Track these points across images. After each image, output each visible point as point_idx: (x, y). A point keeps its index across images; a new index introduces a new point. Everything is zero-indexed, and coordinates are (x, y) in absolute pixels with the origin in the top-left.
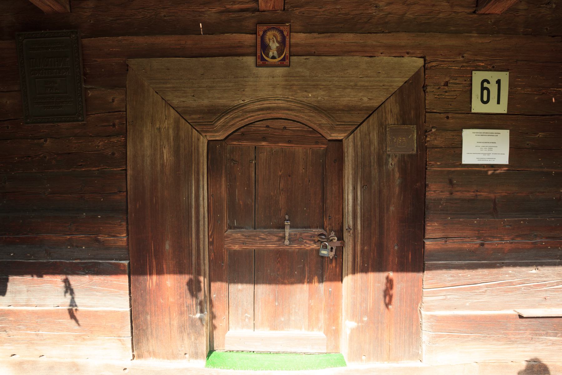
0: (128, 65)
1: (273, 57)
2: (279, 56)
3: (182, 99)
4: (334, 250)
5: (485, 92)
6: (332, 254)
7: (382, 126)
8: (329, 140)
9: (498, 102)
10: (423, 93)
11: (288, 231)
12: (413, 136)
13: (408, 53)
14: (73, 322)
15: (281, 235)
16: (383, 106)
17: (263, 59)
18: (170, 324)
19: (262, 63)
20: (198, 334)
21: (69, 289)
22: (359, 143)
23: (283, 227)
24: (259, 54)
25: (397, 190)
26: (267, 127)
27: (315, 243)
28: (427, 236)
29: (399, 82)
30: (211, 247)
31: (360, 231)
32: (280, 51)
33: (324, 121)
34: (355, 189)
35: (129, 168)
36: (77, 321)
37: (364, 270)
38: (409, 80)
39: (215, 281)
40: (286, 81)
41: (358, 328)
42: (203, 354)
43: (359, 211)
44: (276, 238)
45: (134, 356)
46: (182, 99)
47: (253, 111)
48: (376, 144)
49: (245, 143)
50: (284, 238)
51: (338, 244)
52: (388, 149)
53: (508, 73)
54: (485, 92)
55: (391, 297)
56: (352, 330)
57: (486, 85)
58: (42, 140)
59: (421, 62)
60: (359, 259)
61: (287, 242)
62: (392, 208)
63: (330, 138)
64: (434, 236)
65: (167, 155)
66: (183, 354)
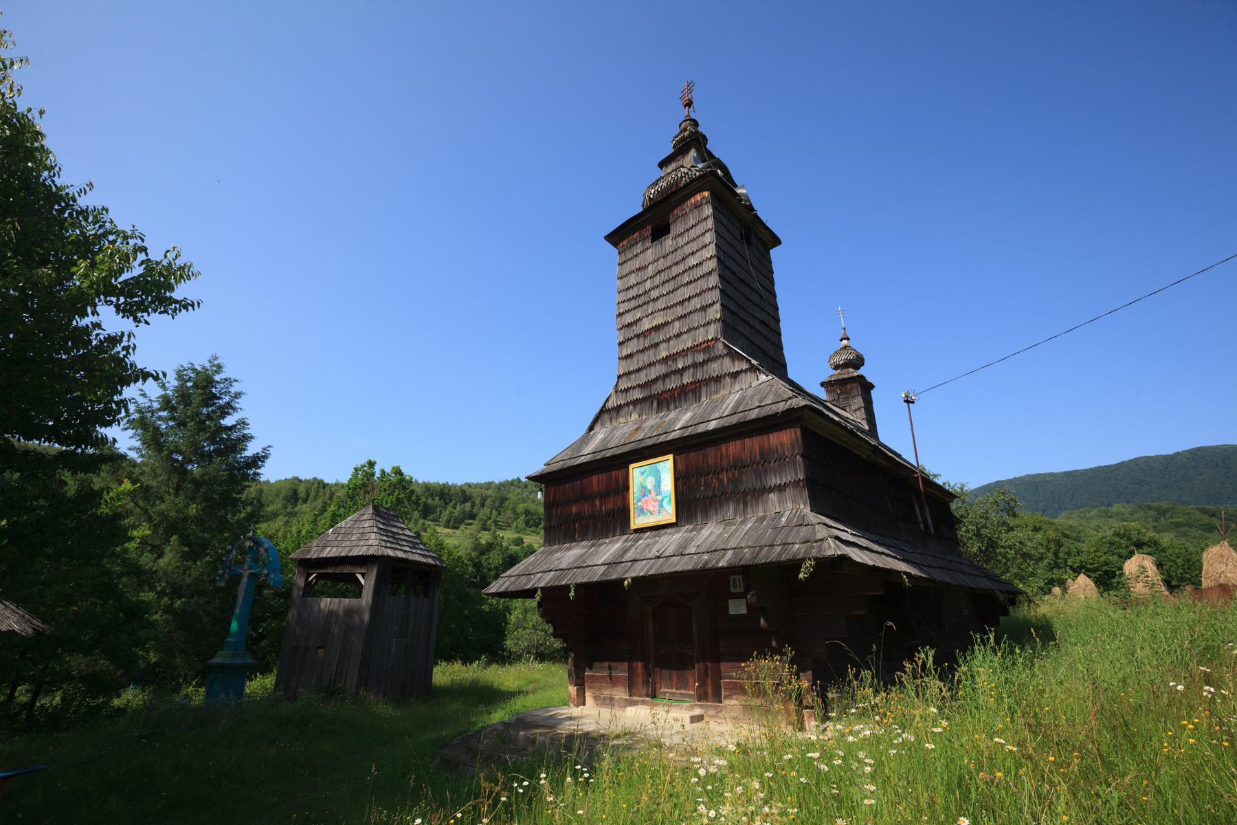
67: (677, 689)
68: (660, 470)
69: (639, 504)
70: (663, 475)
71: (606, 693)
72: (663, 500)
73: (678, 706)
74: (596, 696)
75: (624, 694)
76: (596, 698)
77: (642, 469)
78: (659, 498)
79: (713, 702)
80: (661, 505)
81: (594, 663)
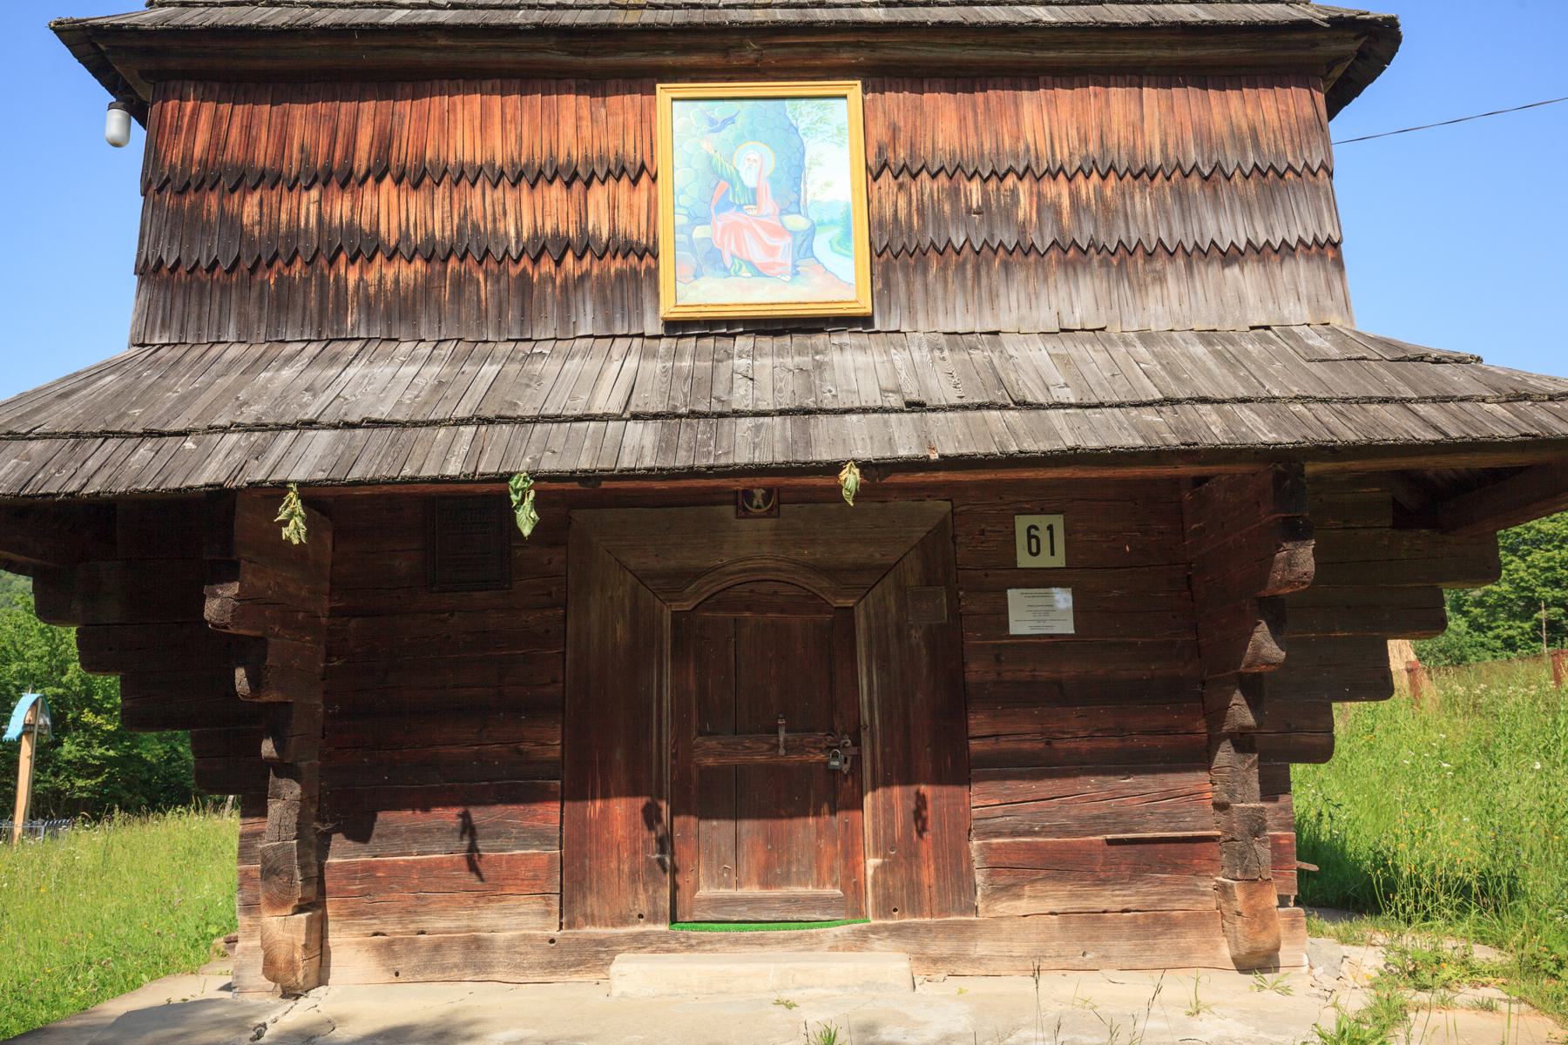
0: (570, 518)
1: (758, 507)
2: (766, 504)
3: (641, 560)
4: (849, 761)
5: (1034, 541)
6: (846, 768)
8: (836, 608)
9: (1053, 554)
10: (952, 546)
11: (782, 735)
12: (942, 600)
13: (929, 496)
14: (474, 876)
15: (774, 741)
16: (901, 563)
17: (745, 509)
18: (619, 869)
19: (744, 513)
20: (657, 880)
21: (468, 829)
22: (872, 612)
23: (777, 732)
24: (740, 501)
25: (925, 671)
26: (752, 591)
27: (822, 751)
28: (972, 733)
29: (920, 532)
30: (674, 762)
31: (878, 728)
33: (825, 584)
34: (869, 671)
35: (568, 650)
36: (479, 874)
37: (888, 783)
38: (934, 529)
39: (678, 814)
40: (776, 535)
41: (884, 864)
42: (665, 914)
43: (875, 699)
44: (766, 747)
45: (561, 924)
46: (641, 560)
47: (732, 573)
48: (455, 750)
49: (721, 614)
50: (777, 746)
51: (854, 751)
52: (910, 618)
53: (1062, 516)
54: (1034, 541)
55: (924, 821)
56: (876, 869)
57: (1033, 532)
58: (447, 615)
60: (879, 766)
61: (782, 752)
62: (919, 696)
63: (835, 605)
64: (981, 732)
65: (621, 631)
66: (636, 915)
67: (765, 884)
68: (802, 126)
69: (700, 232)
70: (813, 148)
71: (442, 924)
72: (812, 232)
73: (798, 938)
74: (390, 944)
75: (538, 921)
76: (387, 950)
78: (796, 222)
79: (944, 912)
80: (804, 245)
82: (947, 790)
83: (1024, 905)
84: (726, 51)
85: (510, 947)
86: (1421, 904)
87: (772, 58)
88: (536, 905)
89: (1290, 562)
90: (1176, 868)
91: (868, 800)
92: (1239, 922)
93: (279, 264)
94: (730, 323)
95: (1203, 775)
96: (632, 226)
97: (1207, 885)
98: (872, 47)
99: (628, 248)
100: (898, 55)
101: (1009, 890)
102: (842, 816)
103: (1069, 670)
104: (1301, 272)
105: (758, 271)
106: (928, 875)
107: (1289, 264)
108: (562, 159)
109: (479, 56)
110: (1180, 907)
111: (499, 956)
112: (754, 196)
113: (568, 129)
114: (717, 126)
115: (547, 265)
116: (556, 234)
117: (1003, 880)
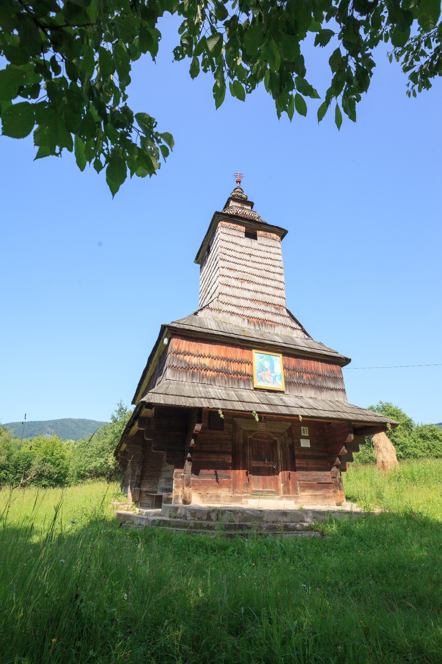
7: (285, 437)
21: (216, 474)
29: (287, 428)
32: (264, 419)
37: (284, 470)
59: (291, 424)
72: (275, 377)
74: (202, 496)
77: (262, 355)
78: (273, 375)
79: (293, 494)
80: (275, 379)
81: (309, 440)
82: (294, 472)
83: (306, 493)
84: (263, 346)
85: (224, 497)
86: (437, 452)
87: (270, 348)
88: (227, 490)
89: (350, 437)
90: (327, 488)
91: (280, 473)
92: (338, 497)
93: (193, 369)
94: (264, 389)
95: (329, 472)
96: (248, 371)
97: (331, 491)
98: (284, 350)
99: (248, 375)
100: (287, 351)
101: (303, 491)
102: (275, 476)
103: (310, 453)
104: (340, 393)
105: (268, 382)
106: (291, 487)
107: (339, 392)
108: (238, 359)
109: (227, 341)
110: (328, 495)
111: (222, 499)
112: (267, 369)
113: (239, 354)
114: (261, 358)
115: (235, 376)
116: (237, 371)
117: (302, 489)
